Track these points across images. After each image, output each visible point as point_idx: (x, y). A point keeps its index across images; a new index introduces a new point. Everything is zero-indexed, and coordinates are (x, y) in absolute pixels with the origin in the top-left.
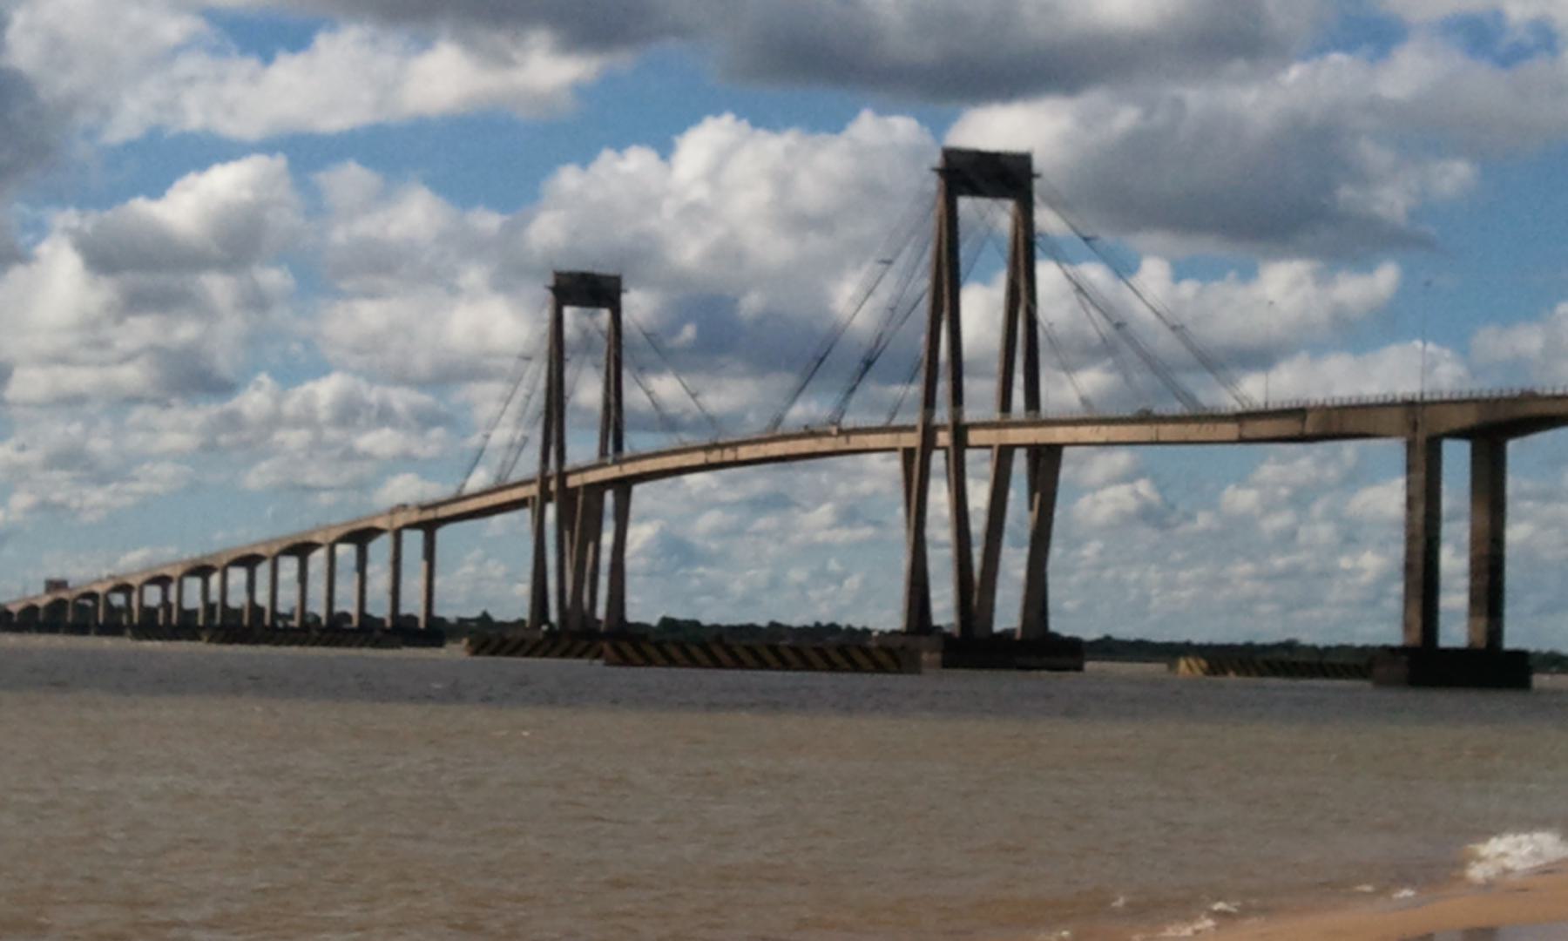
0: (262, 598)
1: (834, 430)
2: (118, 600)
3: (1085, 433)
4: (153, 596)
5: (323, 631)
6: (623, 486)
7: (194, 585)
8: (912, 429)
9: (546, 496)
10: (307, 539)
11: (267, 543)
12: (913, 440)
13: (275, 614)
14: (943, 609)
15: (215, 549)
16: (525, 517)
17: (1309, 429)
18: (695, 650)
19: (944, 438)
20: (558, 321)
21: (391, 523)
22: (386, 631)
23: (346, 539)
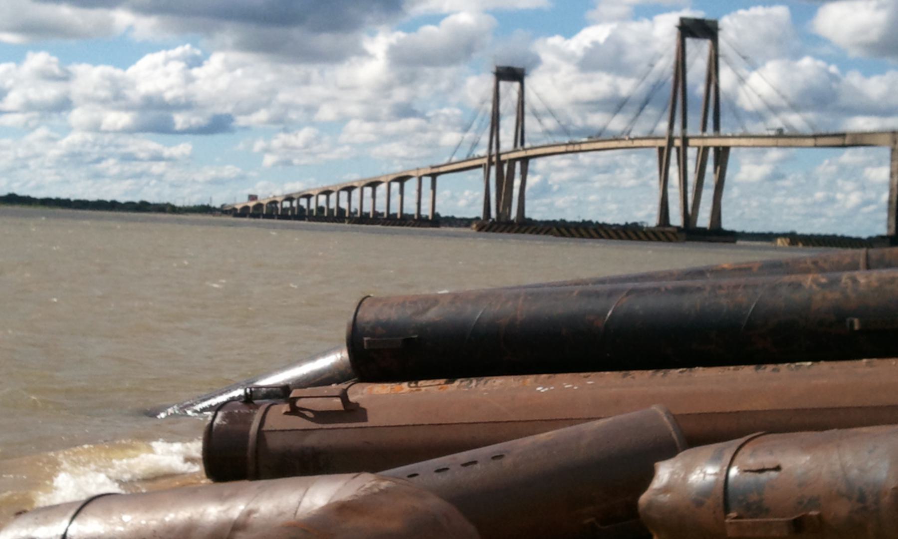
1: (627, 138)
2: (303, 202)
3: (743, 141)
4: (287, 204)
6: (525, 160)
8: (663, 138)
9: (491, 163)
10: (378, 180)
12: (664, 143)
16: (481, 171)
18: (563, 230)
19: (678, 143)
20: (497, 88)
21: (418, 174)
22: (415, 220)
23: (395, 180)
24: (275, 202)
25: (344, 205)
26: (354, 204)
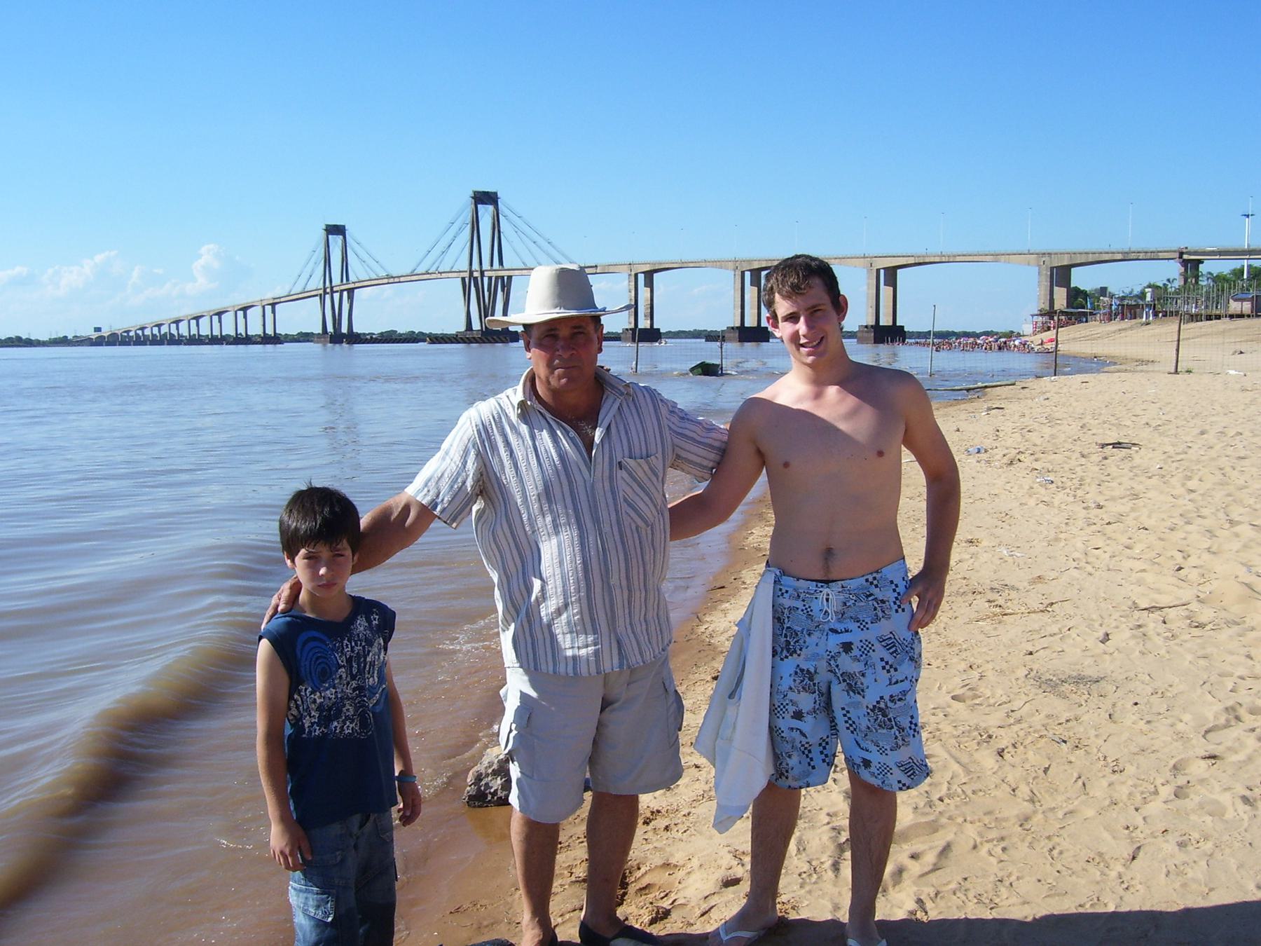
0: (175, 333)
2: (156, 331)
6: (351, 292)
9: (325, 293)
13: (199, 335)
14: (330, 329)
24: (128, 332)
25: (174, 331)
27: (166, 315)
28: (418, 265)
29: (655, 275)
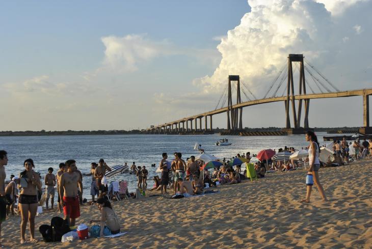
0: (185, 128)
2: (163, 128)
5: (195, 132)
6: (241, 108)
7: (174, 126)
9: (229, 110)
11: (205, 113)
14: (292, 125)
15: (178, 120)
16: (226, 112)
17: (348, 95)
26: (189, 126)
27: (170, 120)
28: (266, 95)
29: (243, 108)
